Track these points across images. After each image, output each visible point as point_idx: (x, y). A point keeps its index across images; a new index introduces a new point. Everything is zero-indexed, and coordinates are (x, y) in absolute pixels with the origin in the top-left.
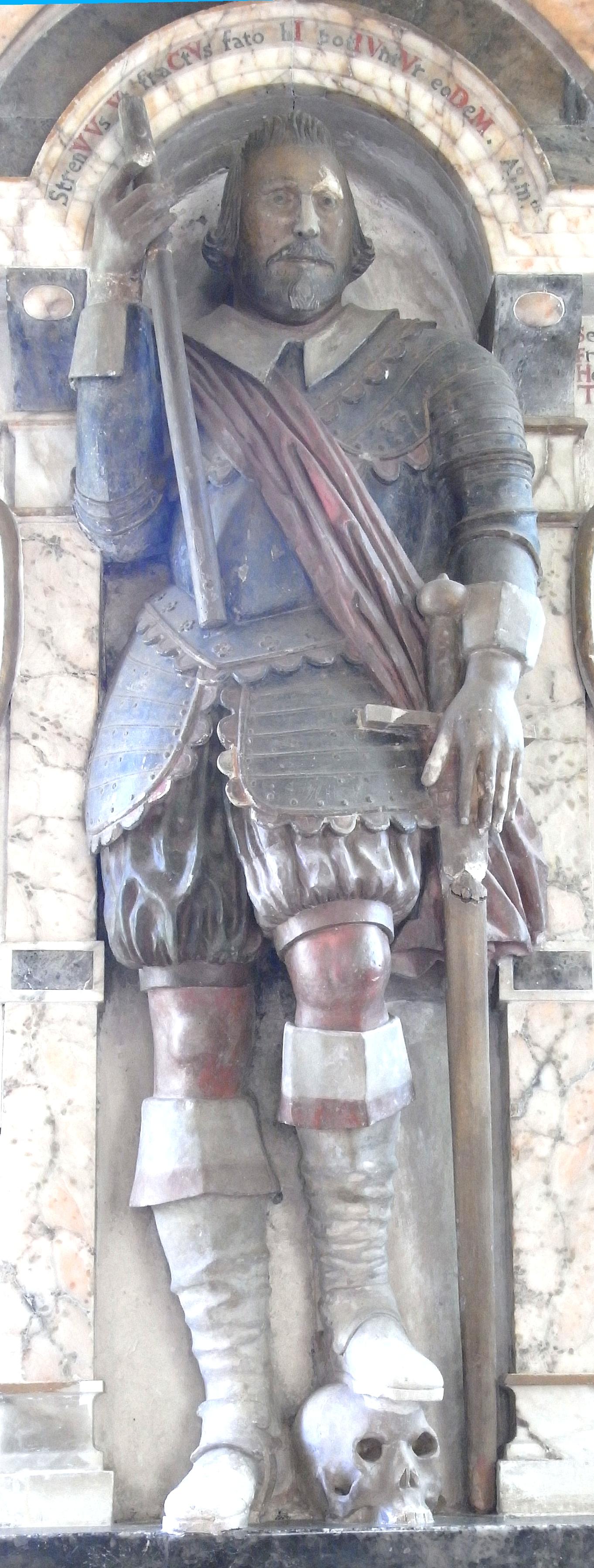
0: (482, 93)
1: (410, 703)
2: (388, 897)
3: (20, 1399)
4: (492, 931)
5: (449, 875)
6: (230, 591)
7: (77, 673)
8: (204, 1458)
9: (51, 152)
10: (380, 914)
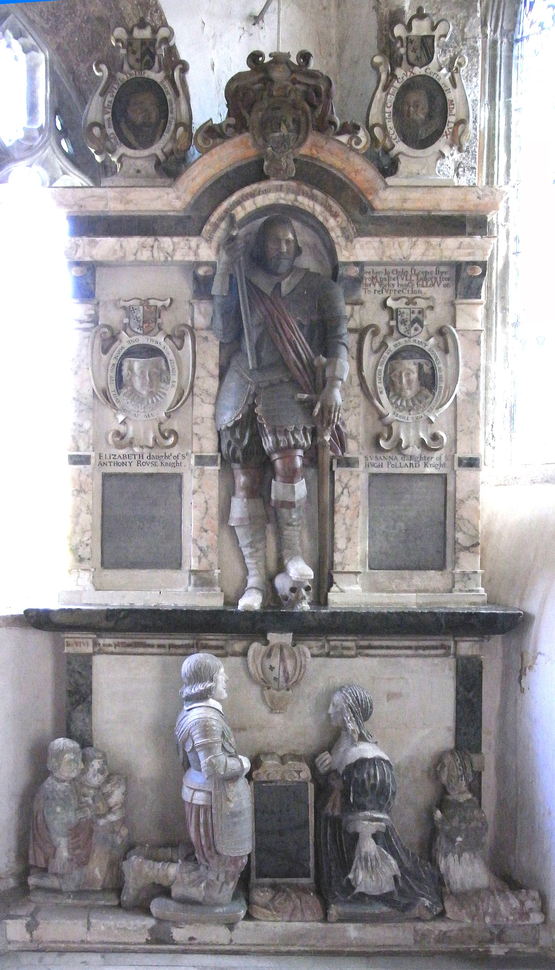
0: (336, 207)
1: (310, 393)
2: (302, 448)
3: (198, 574)
4: (331, 453)
5: (319, 439)
6: (259, 359)
7: (212, 376)
8: (250, 591)
9: (207, 227)
10: (300, 452)
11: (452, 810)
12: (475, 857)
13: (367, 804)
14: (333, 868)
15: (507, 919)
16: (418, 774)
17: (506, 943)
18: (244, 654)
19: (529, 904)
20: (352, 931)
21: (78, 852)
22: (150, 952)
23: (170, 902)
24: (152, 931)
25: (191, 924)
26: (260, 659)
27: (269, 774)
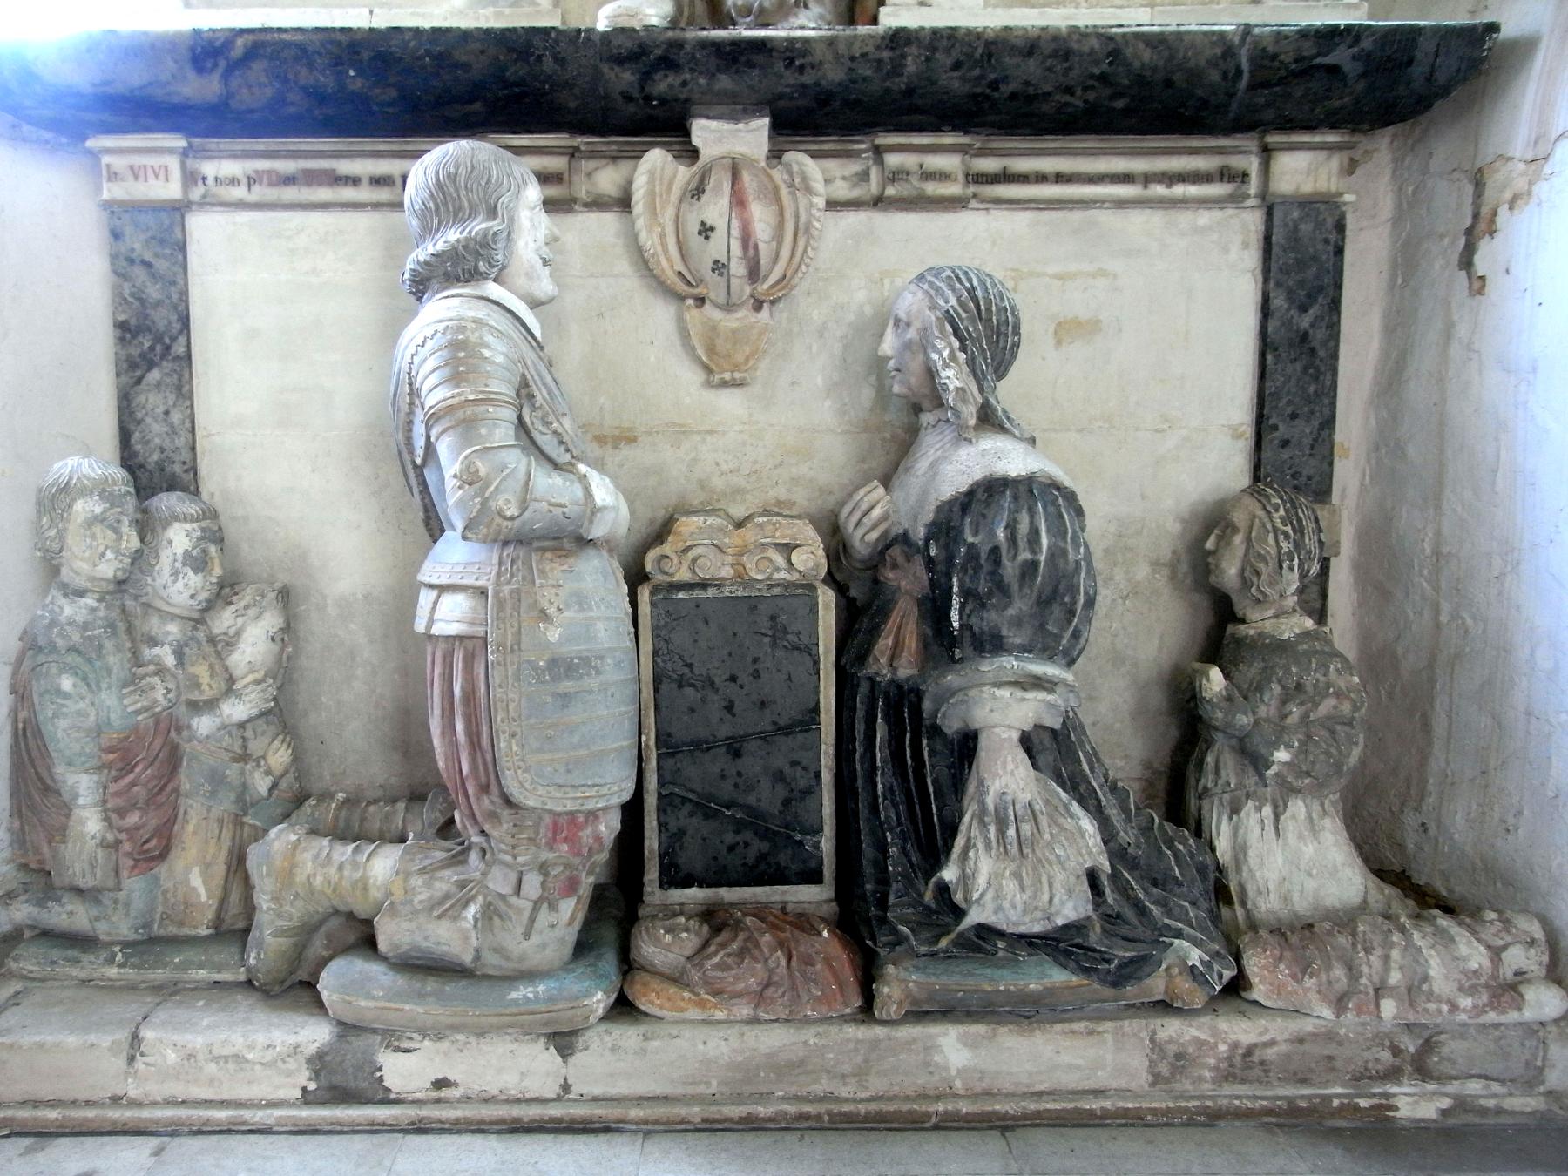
11: (1257, 666)
12: (1325, 813)
13: (1004, 632)
14: (893, 850)
15: (1454, 1007)
16: (1142, 572)
17: (1440, 1079)
18: (624, 203)
19: (1517, 958)
20: (955, 1051)
21: (133, 819)
22: (312, 1130)
23: (375, 969)
24: (319, 1063)
25: (439, 1037)
26: (670, 211)
27: (694, 560)
